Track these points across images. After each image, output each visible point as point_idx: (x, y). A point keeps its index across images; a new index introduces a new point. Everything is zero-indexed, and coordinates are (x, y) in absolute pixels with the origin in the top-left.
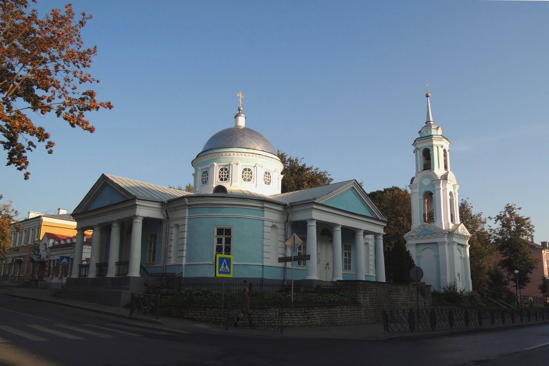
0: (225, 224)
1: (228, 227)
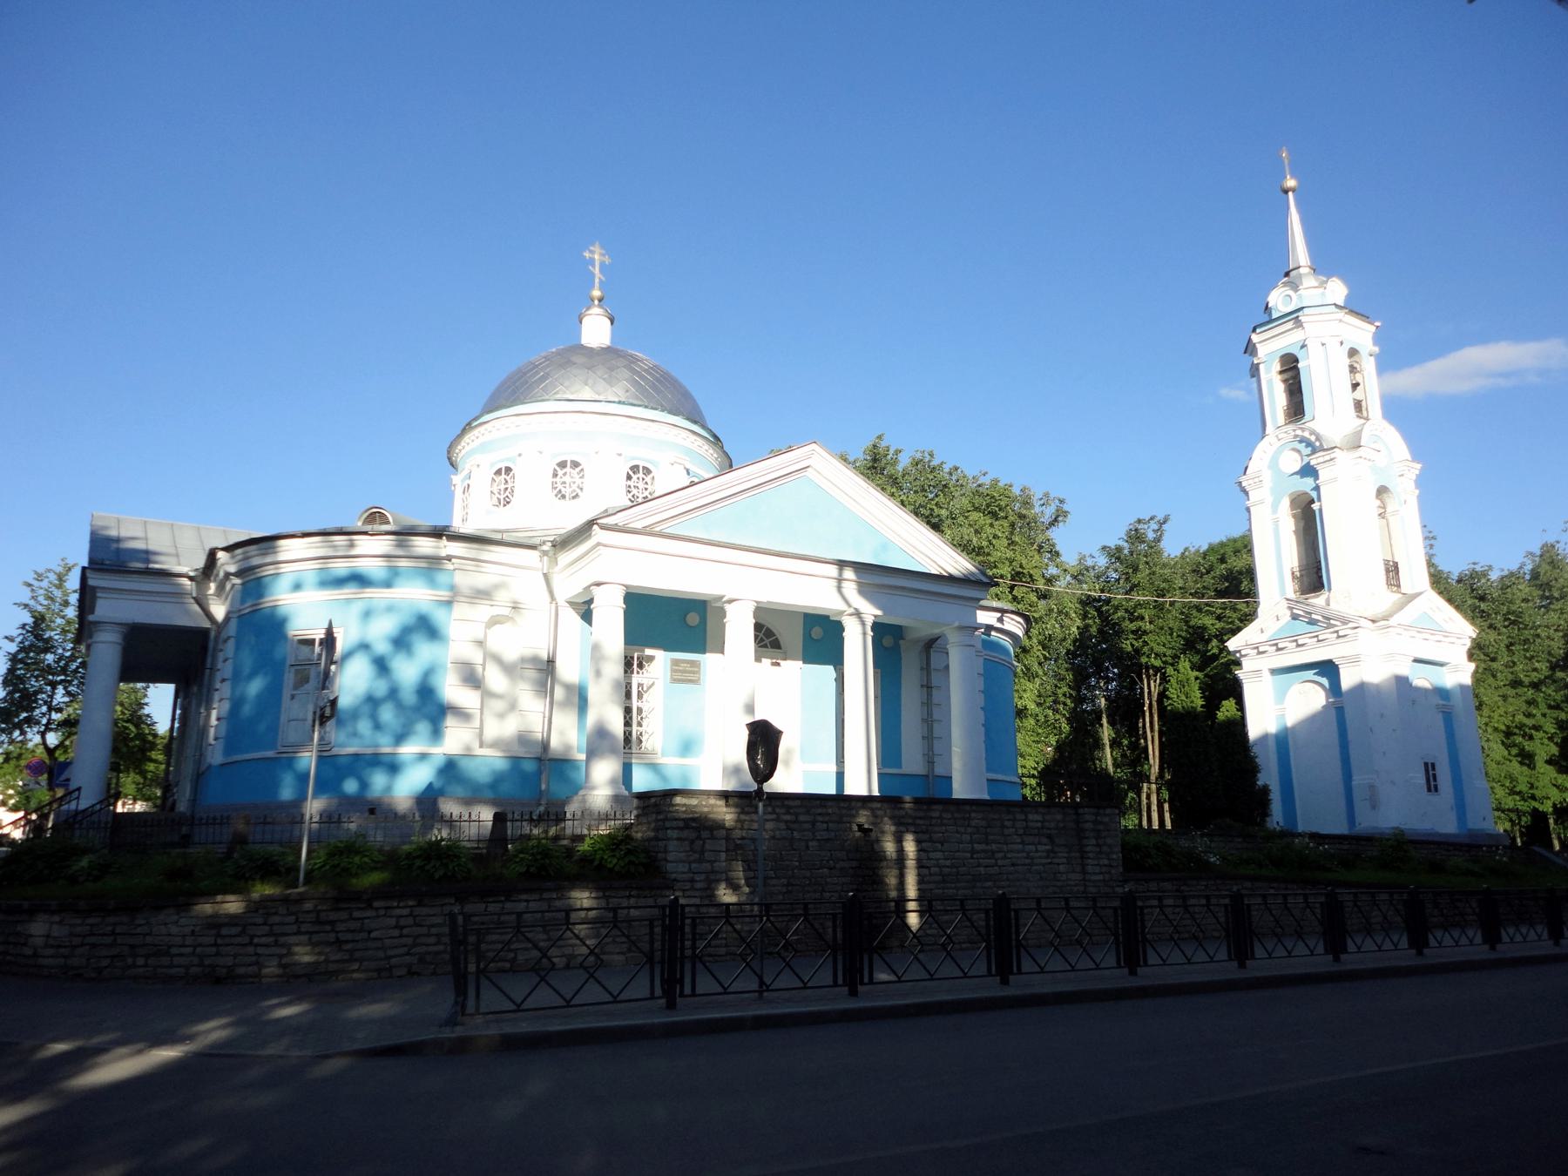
0: (1433, 798)
1: (928, 631)
